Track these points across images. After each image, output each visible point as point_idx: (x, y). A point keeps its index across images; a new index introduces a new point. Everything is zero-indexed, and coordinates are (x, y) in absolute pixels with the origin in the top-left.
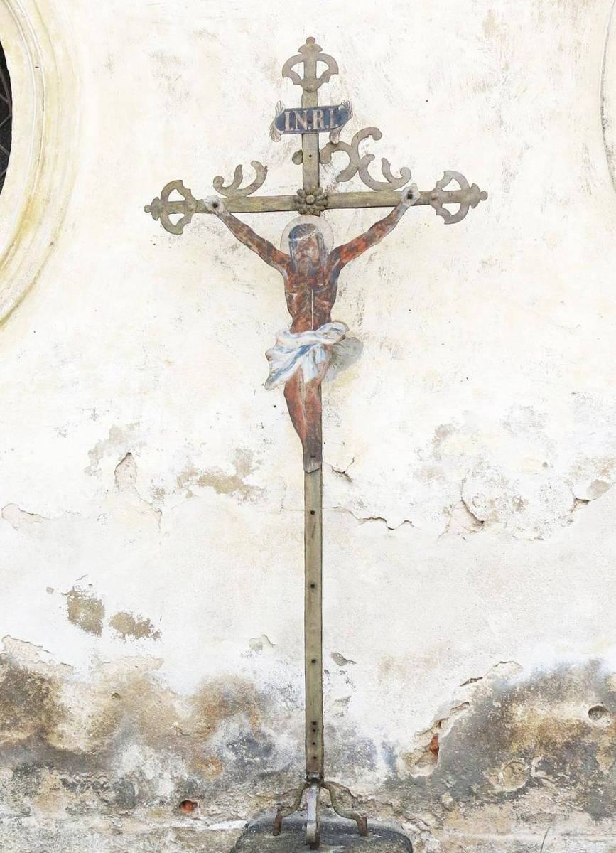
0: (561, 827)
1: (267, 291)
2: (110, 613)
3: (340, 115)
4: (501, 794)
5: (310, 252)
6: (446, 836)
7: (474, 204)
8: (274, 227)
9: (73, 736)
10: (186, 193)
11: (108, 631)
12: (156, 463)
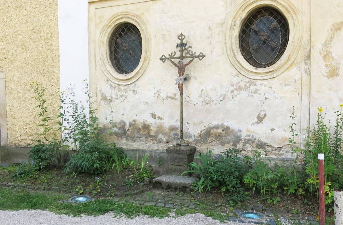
0: (217, 147)
1: (175, 71)
2: (157, 116)
3: (185, 44)
4: (209, 142)
5: (181, 65)
6: (201, 147)
7: (204, 57)
8: (177, 61)
9: (153, 133)
10: (165, 56)
11: (157, 119)
12: (163, 95)
